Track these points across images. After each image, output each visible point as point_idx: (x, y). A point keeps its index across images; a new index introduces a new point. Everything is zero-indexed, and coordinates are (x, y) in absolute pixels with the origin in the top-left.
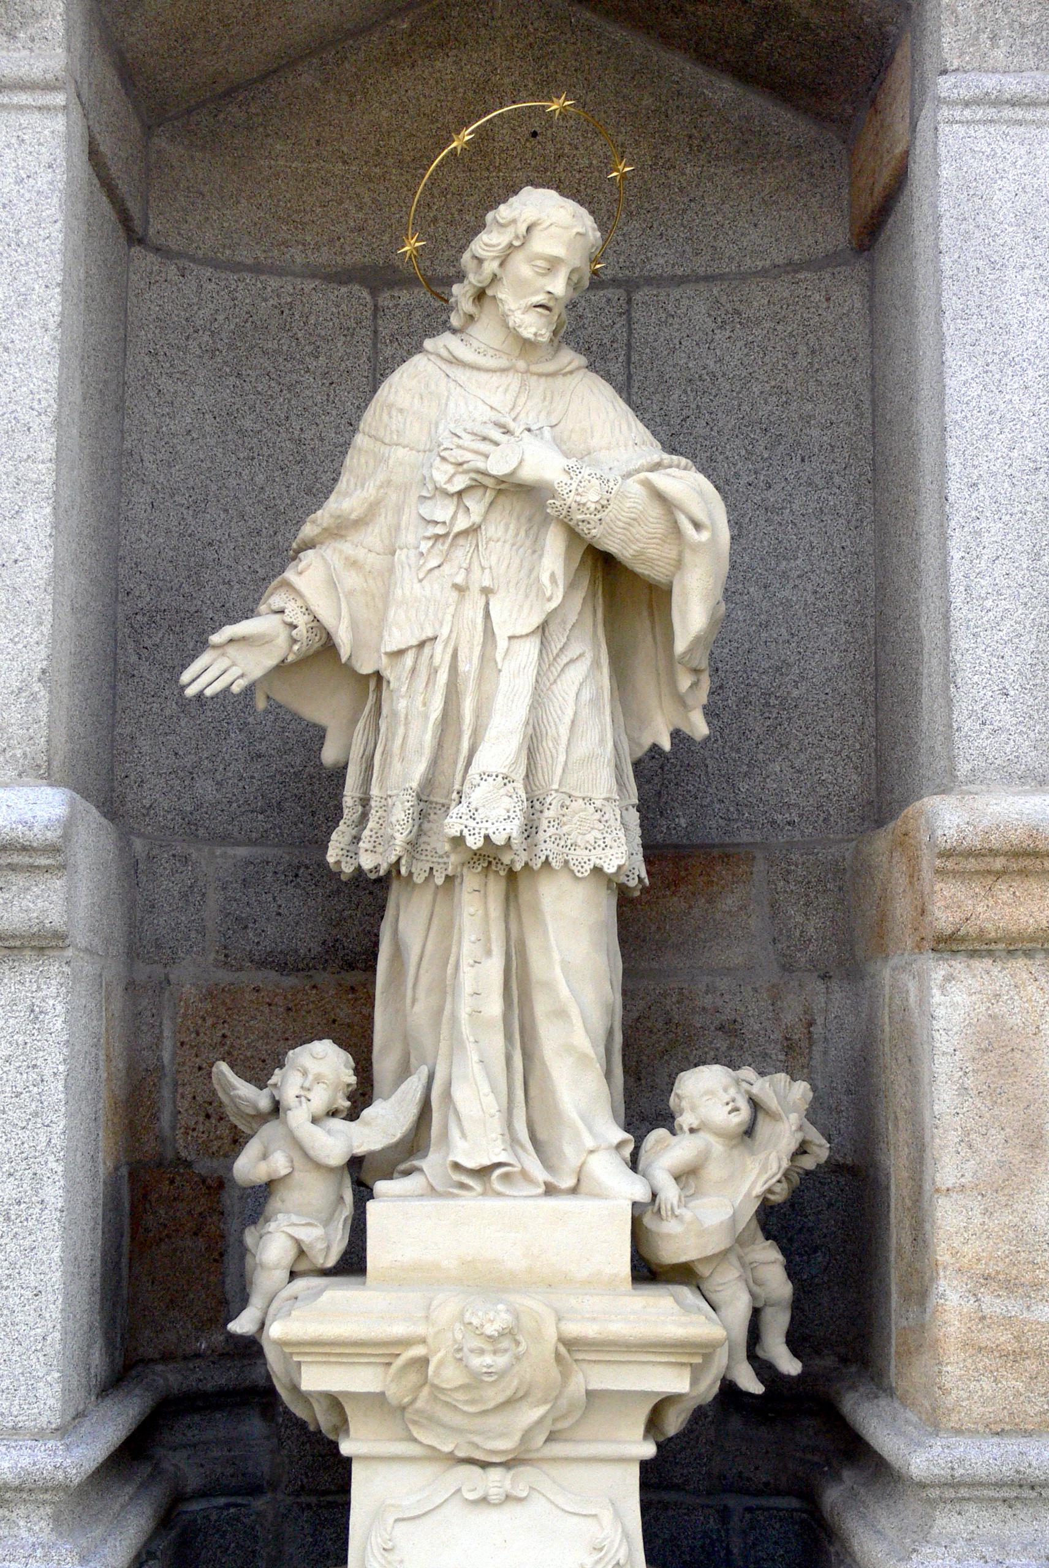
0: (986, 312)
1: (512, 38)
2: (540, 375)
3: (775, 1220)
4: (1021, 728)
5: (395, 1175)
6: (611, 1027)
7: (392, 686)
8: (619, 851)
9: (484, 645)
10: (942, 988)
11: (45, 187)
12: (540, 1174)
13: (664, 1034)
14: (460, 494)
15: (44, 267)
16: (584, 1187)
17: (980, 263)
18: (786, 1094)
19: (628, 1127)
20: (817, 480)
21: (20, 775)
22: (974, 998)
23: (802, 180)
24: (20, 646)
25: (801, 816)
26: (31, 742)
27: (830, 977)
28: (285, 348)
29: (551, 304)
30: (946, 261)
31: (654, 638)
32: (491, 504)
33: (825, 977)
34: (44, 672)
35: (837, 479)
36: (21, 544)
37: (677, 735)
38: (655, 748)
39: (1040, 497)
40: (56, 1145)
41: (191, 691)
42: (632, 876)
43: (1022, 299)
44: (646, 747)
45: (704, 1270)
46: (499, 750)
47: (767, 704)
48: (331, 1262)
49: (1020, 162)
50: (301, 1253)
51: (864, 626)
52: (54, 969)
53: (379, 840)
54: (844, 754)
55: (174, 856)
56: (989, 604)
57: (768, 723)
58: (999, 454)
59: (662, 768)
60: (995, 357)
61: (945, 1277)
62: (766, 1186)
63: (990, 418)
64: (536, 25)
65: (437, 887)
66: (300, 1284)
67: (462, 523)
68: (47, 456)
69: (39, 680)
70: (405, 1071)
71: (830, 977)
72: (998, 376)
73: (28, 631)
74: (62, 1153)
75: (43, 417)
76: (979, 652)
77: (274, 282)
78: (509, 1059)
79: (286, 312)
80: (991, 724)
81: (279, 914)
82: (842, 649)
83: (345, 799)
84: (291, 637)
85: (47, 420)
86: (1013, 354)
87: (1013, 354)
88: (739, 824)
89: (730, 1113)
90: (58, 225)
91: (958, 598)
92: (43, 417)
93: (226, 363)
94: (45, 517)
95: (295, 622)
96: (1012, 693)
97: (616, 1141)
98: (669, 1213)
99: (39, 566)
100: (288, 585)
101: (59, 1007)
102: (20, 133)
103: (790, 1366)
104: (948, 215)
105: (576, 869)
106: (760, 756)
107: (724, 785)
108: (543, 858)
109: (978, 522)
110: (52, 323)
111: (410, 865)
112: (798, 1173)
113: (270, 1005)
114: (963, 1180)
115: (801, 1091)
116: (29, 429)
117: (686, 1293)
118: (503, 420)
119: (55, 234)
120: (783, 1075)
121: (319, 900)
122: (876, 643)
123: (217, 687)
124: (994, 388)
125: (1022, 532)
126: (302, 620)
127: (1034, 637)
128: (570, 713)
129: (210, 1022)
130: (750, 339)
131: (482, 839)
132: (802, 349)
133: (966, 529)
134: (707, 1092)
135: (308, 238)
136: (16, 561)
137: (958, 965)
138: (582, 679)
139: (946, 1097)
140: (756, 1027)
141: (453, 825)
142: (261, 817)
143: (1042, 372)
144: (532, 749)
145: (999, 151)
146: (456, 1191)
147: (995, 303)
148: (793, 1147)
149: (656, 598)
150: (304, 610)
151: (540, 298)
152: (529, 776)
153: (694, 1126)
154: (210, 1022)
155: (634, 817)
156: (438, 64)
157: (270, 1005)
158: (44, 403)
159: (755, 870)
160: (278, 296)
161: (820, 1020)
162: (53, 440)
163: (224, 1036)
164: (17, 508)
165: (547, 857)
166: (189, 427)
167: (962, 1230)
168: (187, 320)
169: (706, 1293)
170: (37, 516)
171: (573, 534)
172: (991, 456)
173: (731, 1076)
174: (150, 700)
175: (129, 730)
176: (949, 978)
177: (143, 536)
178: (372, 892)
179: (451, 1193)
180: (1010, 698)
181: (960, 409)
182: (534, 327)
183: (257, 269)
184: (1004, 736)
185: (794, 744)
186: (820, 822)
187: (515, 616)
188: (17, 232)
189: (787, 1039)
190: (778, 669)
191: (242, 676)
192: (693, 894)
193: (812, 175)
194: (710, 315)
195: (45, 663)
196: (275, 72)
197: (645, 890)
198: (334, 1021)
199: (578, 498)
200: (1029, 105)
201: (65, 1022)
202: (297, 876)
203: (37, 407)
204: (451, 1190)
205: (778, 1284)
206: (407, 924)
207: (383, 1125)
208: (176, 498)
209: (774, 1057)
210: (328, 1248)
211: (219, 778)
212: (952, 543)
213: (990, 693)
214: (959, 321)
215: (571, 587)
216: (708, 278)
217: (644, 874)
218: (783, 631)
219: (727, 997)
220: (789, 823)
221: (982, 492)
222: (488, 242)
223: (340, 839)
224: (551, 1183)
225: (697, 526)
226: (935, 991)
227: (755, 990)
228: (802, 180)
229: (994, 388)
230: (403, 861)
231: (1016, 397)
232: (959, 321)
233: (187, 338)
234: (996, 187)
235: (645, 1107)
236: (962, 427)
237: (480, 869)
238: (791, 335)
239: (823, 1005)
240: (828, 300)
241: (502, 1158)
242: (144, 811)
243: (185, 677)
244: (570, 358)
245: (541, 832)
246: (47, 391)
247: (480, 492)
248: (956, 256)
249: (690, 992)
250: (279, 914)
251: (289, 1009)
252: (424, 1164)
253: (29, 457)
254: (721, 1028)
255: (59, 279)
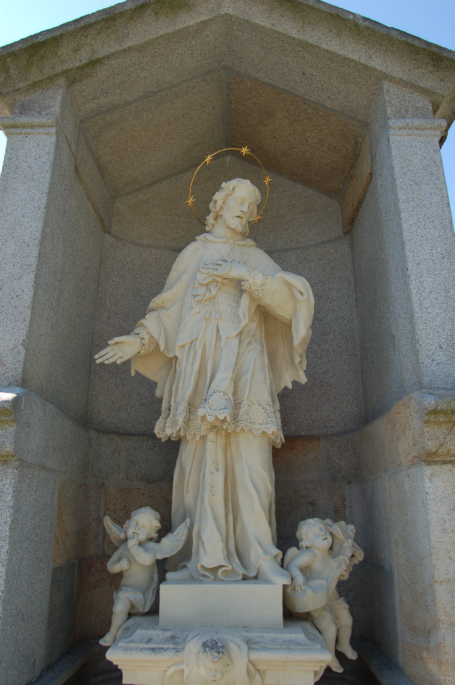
0: (415, 200)
1: (231, 176)
2: (239, 245)
3: (343, 588)
4: (449, 362)
5: (179, 568)
6: (271, 502)
7: (180, 360)
8: (273, 428)
9: (216, 341)
10: (430, 479)
11: (46, 160)
12: (241, 571)
13: (289, 506)
14: (207, 285)
15: (42, 187)
16: (260, 576)
17: (411, 183)
18: (345, 532)
19: (278, 547)
20: (336, 308)
21: (9, 385)
22: (445, 483)
23: (325, 217)
24: (15, 330)
25: (336, 424)
26: (16, 370)
27: (351, 483)
28: (157, 271)
29: (242, 216)
30: (398, 182)
31: (284, 346)
32: (220, 288)
33: (349, 482)
34: (24, 341)
35: (343, 308)
36: (20, 289)
37: (295, 383)
38: (286, 388)
39: (446, 268)
40: (3, 558)
41: (98, 362)
42: (278, 438)
43: (430, 195)
44: (282, 387)
45: (315, 615)
46: (223, 381)
47: (322, 385)
48: (146, 610)
49: (422, 149)
50: (133, 606)
51: (356, 355)
52: (10, 471)
53: (173, 423)
54: (351, 400)
55: (108, 438)
56: (430, 310)
57: (323, 391)
58: (427, 252)
59: (285, 409)
60: (421, 216)
61: (444, 628)
62: (341, 573)
63: (422, 238)
64: (239, 172)
65: (197, 442)
66: (131, 621)
67: (208, 295)
68: (35, 255)
69: (22, 344)
70: (183, 520)
71: (351, 483)
72: (423, 223)
73: (19, 324)
74: (5, 562)
75: (35, 241)
76: (428, 330)
77: (154, 251)
78: (226, 516)
79: (158, 260)
80: (436, 360)
81: (148, 461)
82: (348, 364)
83: (162, 408)
84: (142, 343)
85: (37, 242)
86: (428, 215)
87: (428, 215)
88: (314, 428)
89: (323, 540)
90: (49, 172)
91: (416, 307)
92: (35, 241)
93: (137, 274)
94: (31, 279)
95: (143, 337)
96: (444, 347)
97: (274, 554)
98: (299, 588)
99: (27, 298)
100: (143, 325)
101: (10, 489)
102: (38, 143)
103: (351, 655)
104: (397, 166)
105: (255, 432)
106: (320, 403)
107: (308, 414)
108: (241, 427)
109: (422, 278)
110: (42, 207)
111: (185, 431)
112: (352, 566)
113: (143, 494)
114: (448, 576)
115: (351, 528)
116: (28, 245)
117: (308, 626)
118: (224, 258)
119: (47, 176)
120: (343, 522)
121: (163, 455)
122: (361, 360)
123: (111, 361)
124: (422, 227)
125: (440, 282)
126: (146, 337)
127: (450, 324)
128: (252, 368)
129: (120, 500)
130: (310, 266)
131: (214, 417)
132: (328, 268)
133: (417, 281)
134: (312, 531)
135: (166, 239)
136: (17, 296)
137: (436, 468)
138: (255, 359)
139: (437, 533)
140: (323, 503)
141: (201, 412)
142: (143, 426)
143: (441, 221)
144: (236, 381)
145: (414, 145)
146: (202, 578)
147: (419, 197)
148: (350, 555)
149: (287, 326)
150: (147, 333)
151: (239, 214)
152: (235, 393)
153: (308, 546)
154: (120, 500)
155: (279, 415)
156: (208, 185)
157: (143, 494)
158: (36, 236)
159: (320, 443)
160: (156, 255)
161: (348, 500)
162: (38, 249)
163: (125, 506)
164: (20, 275)
165: (243, 426)
166: (123, 293)
167: (450, 602)
168: (124, 260)
169: (316, 624)
170: (28, 278)
171: (252, 298)
172: (424, 252)
173: (323, 524)
174: (104, 383)
175: (95, 393)
176: (432, 475)
177: (104, 327)
178: (173, 447)
179: (199, 579)
180: (443, 350)
181: (409, 235)
182: (236, 224)
183: (149, 246)
184: (442, 366)
185: (332, 399)
186: (343, 426)
187: (229, 331)
188: (33, 175)
189: (335, 507)
190: (325, 373)
191: (121, 357)
192: (298, 453)
193: (328, 215)
194: (297, 260)
195: (25, 337)
196: (155, 183)
197: (283, 445)
198: (167, 501)
199: (254, 281)
200: (423, 129)
201: (12, 497)
202: (154, 447)
203: (33, 237)
204: (200, 578)
205: (347, 620)
206: (187, 456)
207: (170, 545)
208: (117, 316)
209: (330, 514)
210: (145, 603)
211: (128, 411)
212: (411, 287)
213: (435, 347)
214: (405, 203)
215: (251, 320)
216: (296, 249)
217: (283, 438)
218: (326, 360)
219: (312, 491)
220: (331, 427)
221: (422, 266)
222: (218, 197)
223: (160, 424)
224: (245, 574)
225: (302, 294)
226: (427, 481)
227: (322, 488)
228: (325, 217)
229: (422, 227)
230: (182, 430)
231: (431, 230)
232: (405, 203)
233: (124, 265)
234: (414, 157)
235: (285, 538)
236: (411, 242)
237: (214, 432)
238: (324, 264)
239: (349, 493)
240: (336, 251)
241: (223, 562)
242: (100, 422)
243: (96, 356)
244: (250, 242)
245: (240, 416)
246: (37, 231)
247: (216, 284)
248: (402, 180)
249: (298, 490)
250: (148, 461)
251: (150, 496)
252: (189, 565)
253: (27, 256)
254: (310, 503)
255: (47, 191)
